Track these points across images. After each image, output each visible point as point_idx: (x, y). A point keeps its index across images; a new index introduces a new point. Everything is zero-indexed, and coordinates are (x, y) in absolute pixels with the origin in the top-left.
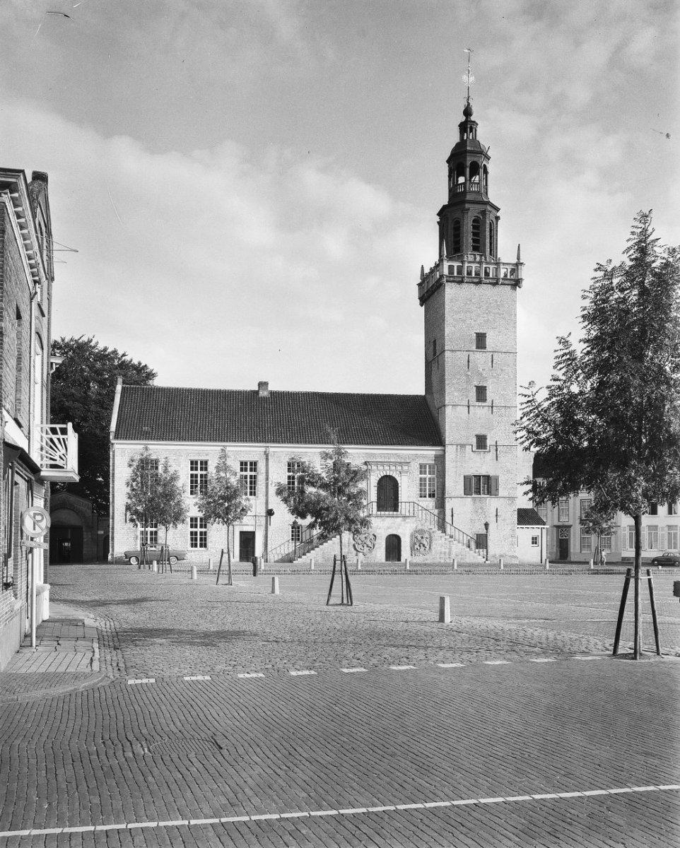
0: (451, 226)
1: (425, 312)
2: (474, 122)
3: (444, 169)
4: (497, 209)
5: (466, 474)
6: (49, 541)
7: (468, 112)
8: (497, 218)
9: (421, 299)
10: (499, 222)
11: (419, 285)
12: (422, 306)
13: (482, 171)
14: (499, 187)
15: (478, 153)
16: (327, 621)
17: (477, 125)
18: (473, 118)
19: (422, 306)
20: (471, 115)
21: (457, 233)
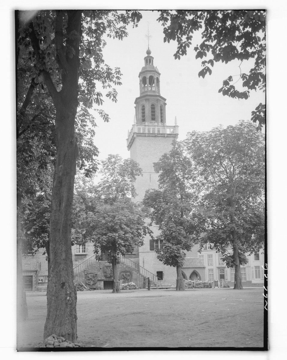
0: (141, 108)
1: (131, 153)
2: (151, 57)
3: (142, 15)
4: (165, 100)
5: (254, 259)
6: (78, 207)
7: (149, 52)
8: (165, 104)
9: (128, 147)
10: (166, 106)
11: (127, 140)
12: (129, 150)
13: (155, 81)
14: (165, 89)
15: (154, 71)
16: (172, 223)
17: (153, 58)
18: (151, 55)
19: (129, 150)
20: (150, 54)
21: (144, 118)
